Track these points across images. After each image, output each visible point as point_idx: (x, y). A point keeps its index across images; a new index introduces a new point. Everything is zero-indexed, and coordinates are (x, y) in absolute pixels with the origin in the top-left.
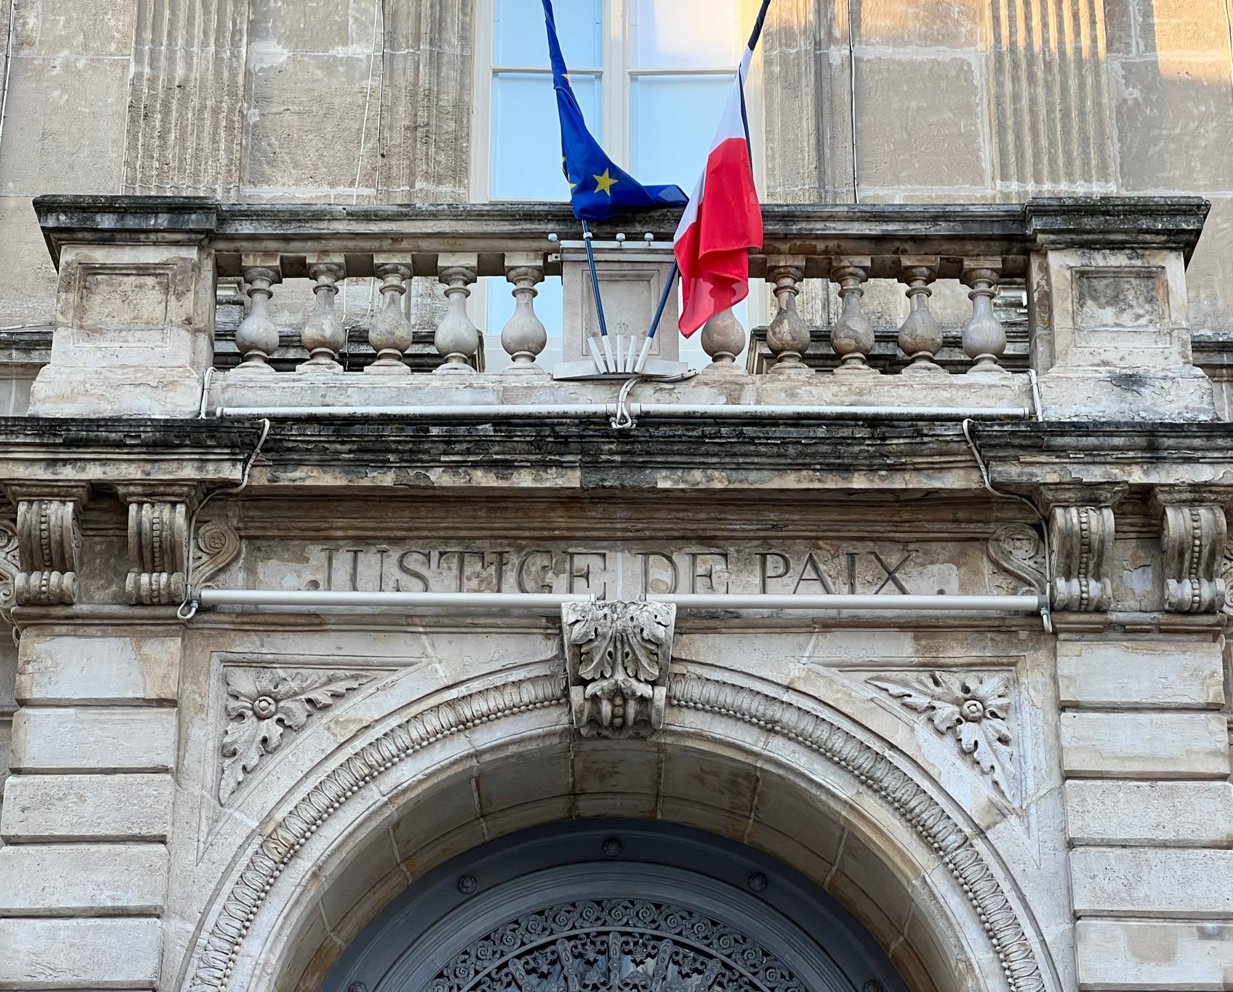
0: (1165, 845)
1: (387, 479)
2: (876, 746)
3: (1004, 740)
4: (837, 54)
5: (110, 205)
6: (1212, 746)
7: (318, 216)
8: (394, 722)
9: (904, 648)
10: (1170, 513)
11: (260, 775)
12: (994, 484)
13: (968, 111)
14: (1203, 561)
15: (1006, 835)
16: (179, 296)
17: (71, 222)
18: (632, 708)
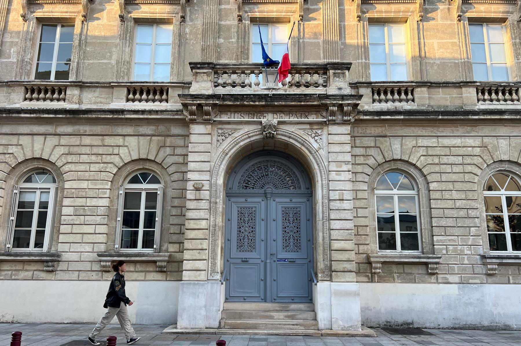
9: (308, 127)
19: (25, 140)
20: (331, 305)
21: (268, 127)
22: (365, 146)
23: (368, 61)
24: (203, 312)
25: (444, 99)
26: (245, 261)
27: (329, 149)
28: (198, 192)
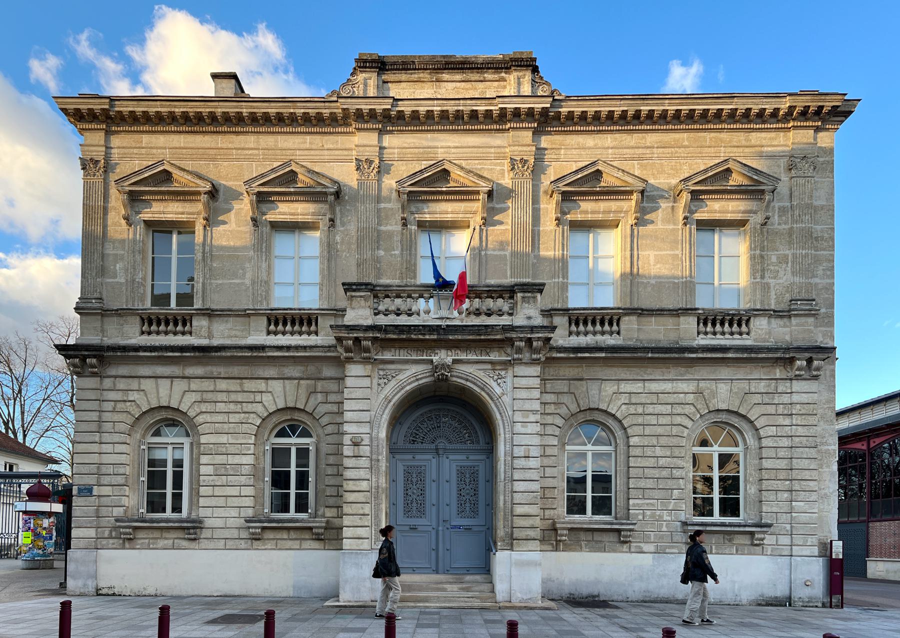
1: (404, 337)
4: (483, 253)
5: (354, 284)
7: (391, 286)
9: (489, 366)
13: (506, 265)
15: (504, 398)
17: (349, 287)
19: (147, 384)
20: (511, 577)
25: (657, 331)
26: (413, 528)
27: (516, 396)
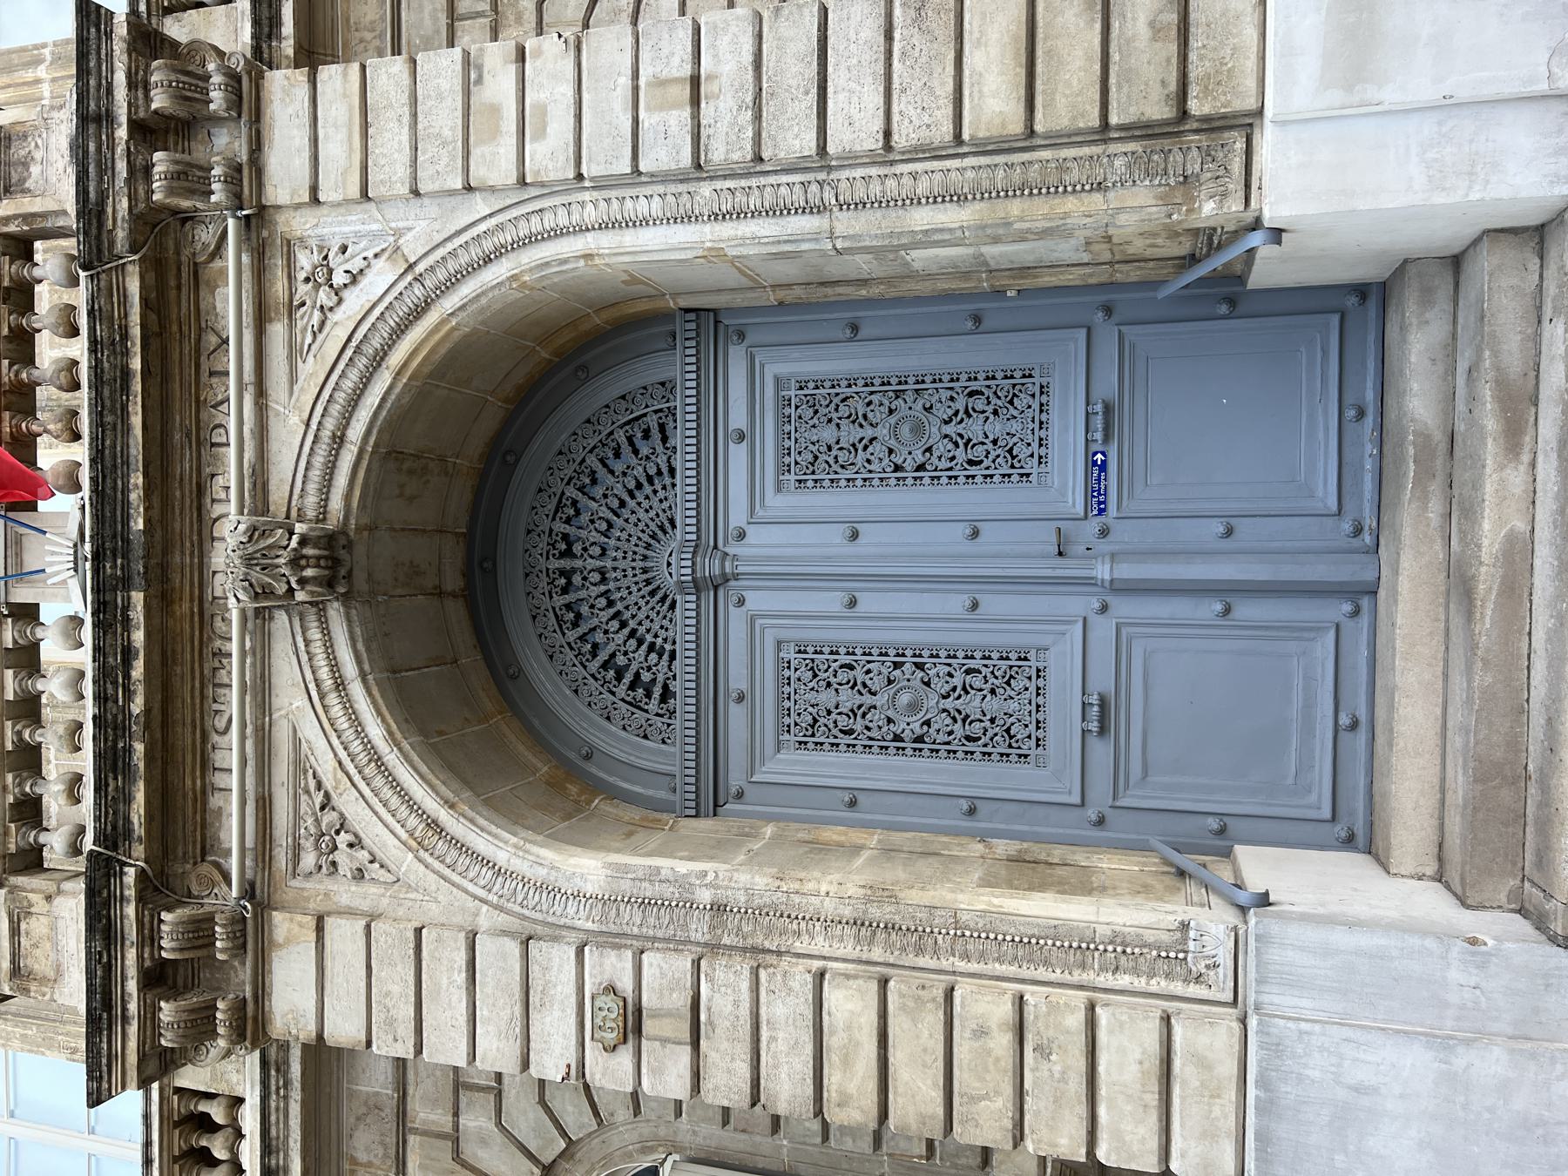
0: (414, 115)
2: (349, 353)
3: (344, 249)
6: (340, 77)
8: (335, 742)
9: (277, 331)
10: (154, 106)
11: (376, 850)
12: (133, 251)
14: (194, 82)
16: (30, 905)
18: (309, 551)
20: (1449, 106)
21: (256, 575)
22: (443, 20)
23: (46, 52)
24: (1490, 1063)
26: (1103, 716)
28: (648, 1026)
